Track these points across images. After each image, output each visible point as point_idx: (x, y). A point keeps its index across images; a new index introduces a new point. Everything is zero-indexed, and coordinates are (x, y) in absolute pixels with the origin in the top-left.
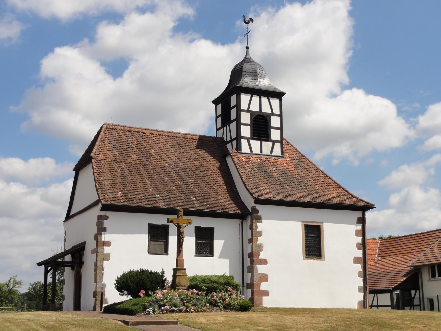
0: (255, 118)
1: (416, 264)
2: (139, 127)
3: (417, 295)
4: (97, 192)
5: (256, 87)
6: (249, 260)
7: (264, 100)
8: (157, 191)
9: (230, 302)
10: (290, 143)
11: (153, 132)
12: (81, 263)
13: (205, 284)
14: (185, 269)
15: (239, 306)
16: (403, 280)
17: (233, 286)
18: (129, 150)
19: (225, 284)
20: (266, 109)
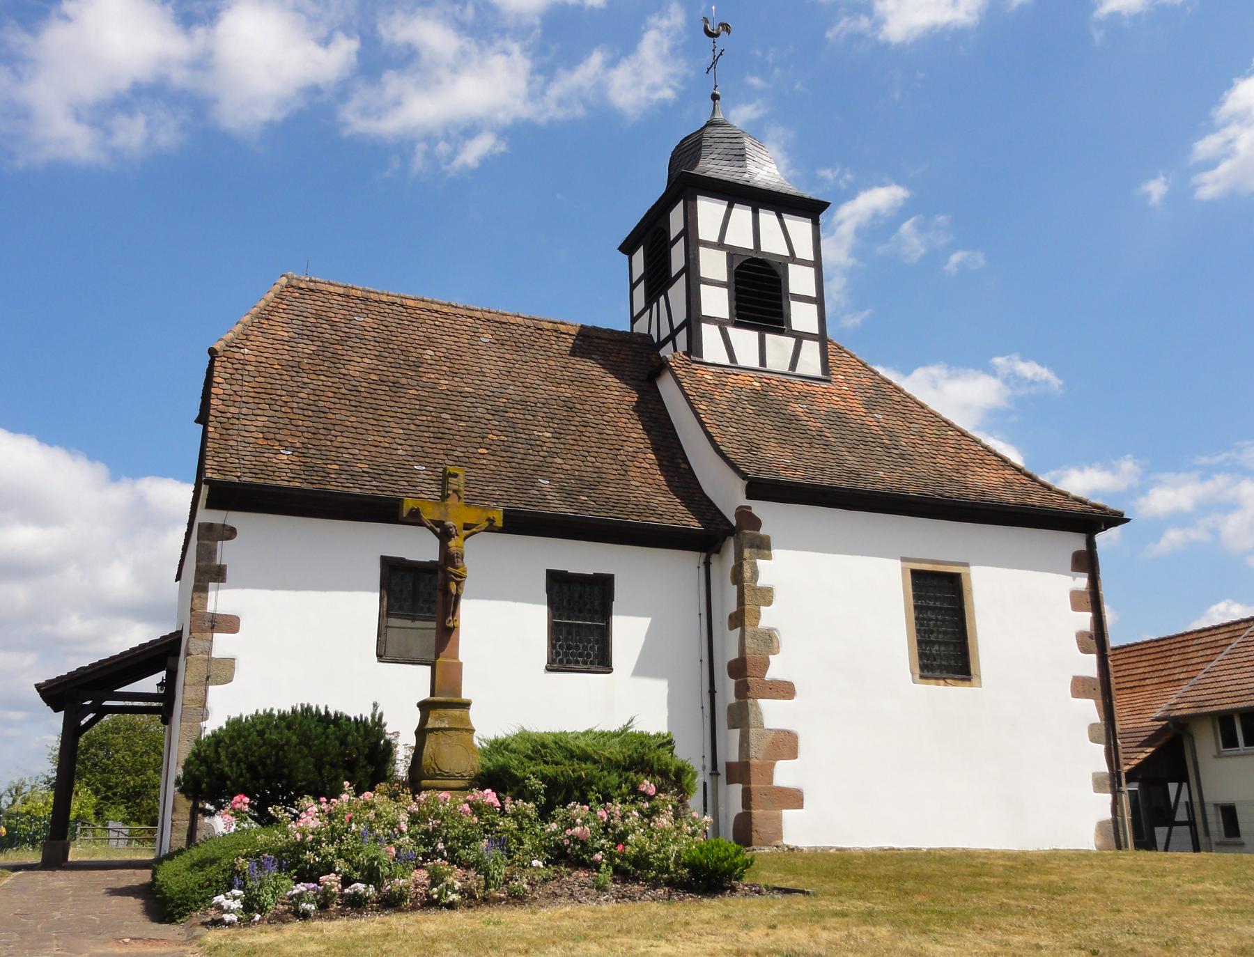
0: (741, 266)
1: (1178, 713)
3: (1184, 797)
6: (731, 683)
7: (768, 218)
8: (423, 457)
9: (642, 849)
11: (435, 307)
13: (542, 767)
14: (466, 705)
15: (685, 865)
16: (1144, 755)
17: (664, 773)
19: (636, 765)
20: (773, 244)
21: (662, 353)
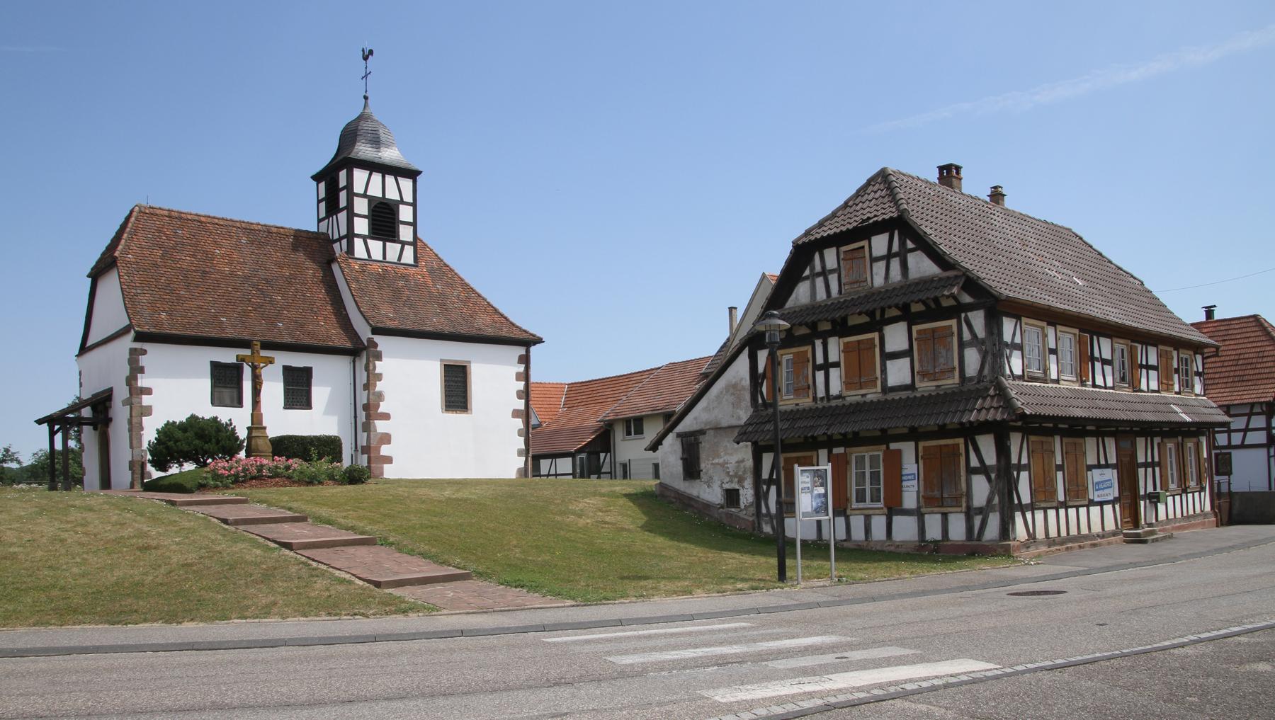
3: (608, 459)
5: (377, 160)
7: (390, 180)
19: (329, 447)
20: (392, 194)
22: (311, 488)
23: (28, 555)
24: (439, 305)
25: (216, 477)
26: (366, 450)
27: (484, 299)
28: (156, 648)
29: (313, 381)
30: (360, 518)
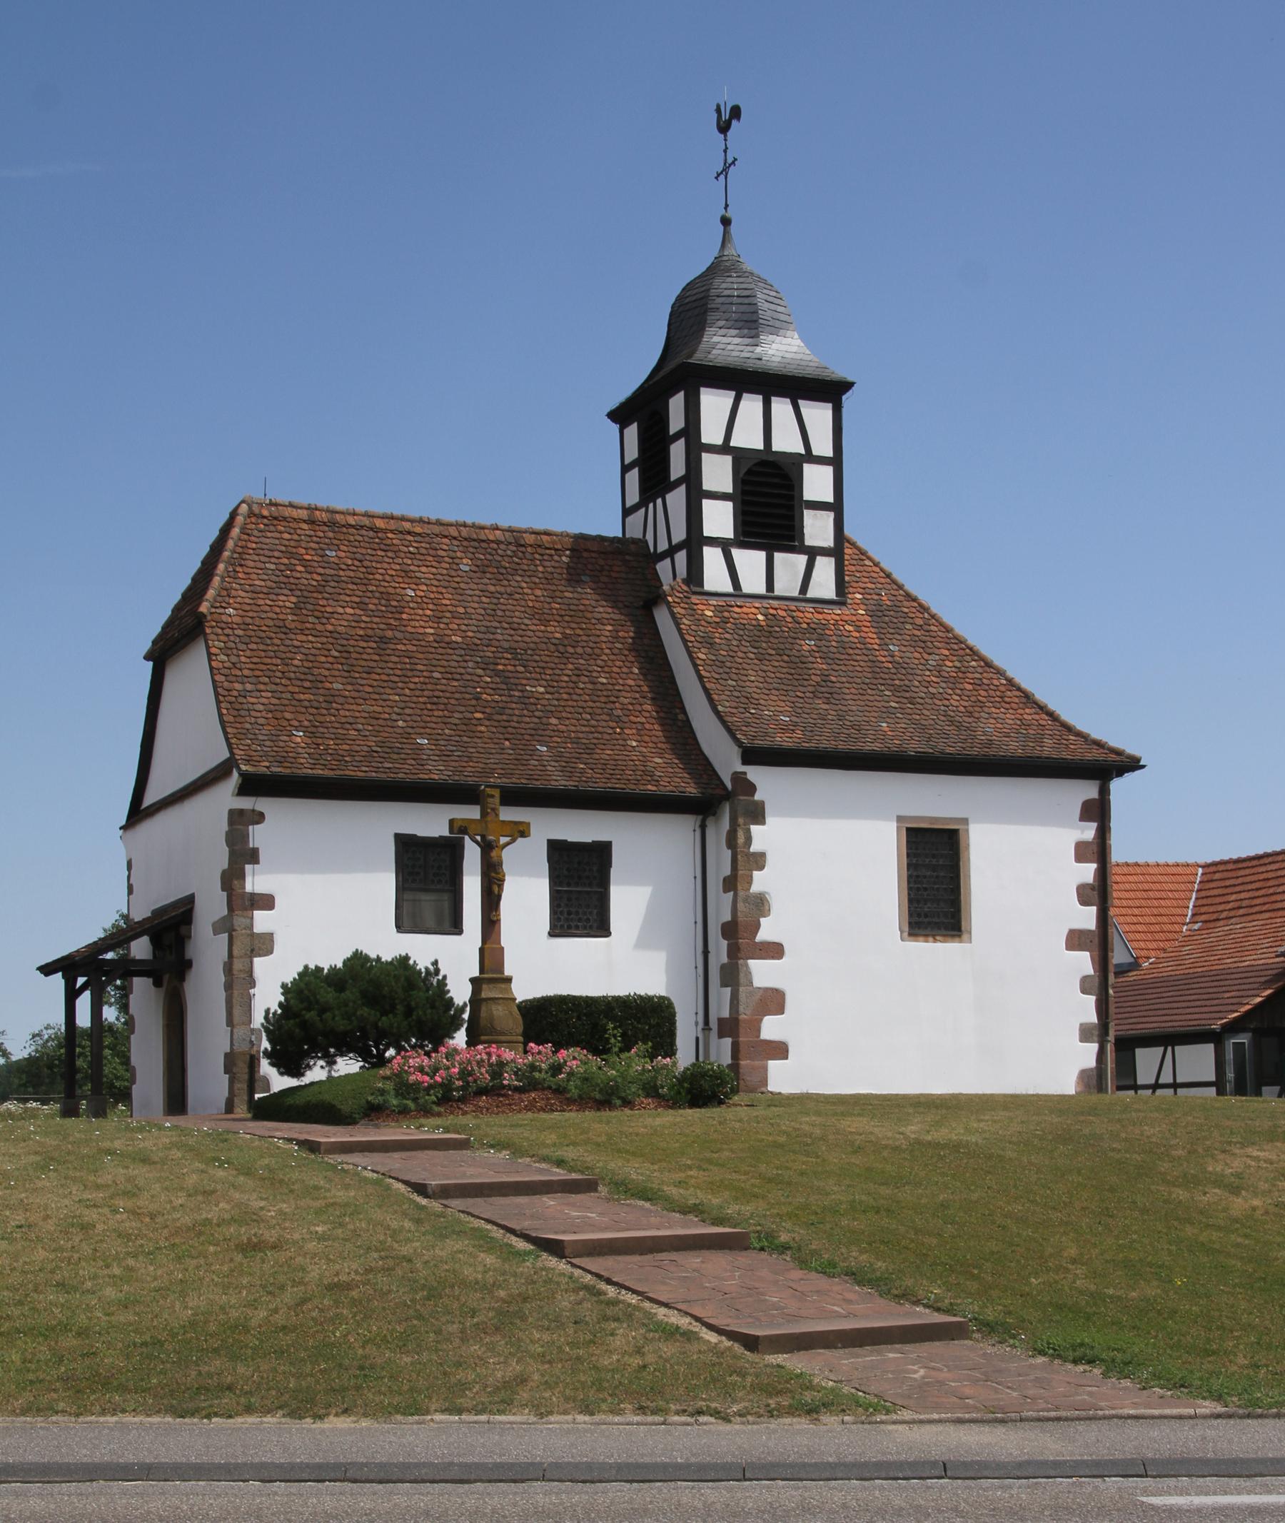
0: (749, 472)
2: (360, 508)
4: (225, 733)
5: (751, 365)
7: (782, 408)
10: (871, 553)
11: (407, 525)
12: (182, 967)
14: (509, 980)
18: (328, 589)
19: (645, 1020)
20: (786, 441)
21: (659, 567)
22: (606, 1114)
23: (16, 1257)
24: (896, 690)
25: (405, 1088)
26: (729, 1027)
27: (1000, 672)
28: (268, 1474)
29: (614, 873)
30: (713, 1187)
